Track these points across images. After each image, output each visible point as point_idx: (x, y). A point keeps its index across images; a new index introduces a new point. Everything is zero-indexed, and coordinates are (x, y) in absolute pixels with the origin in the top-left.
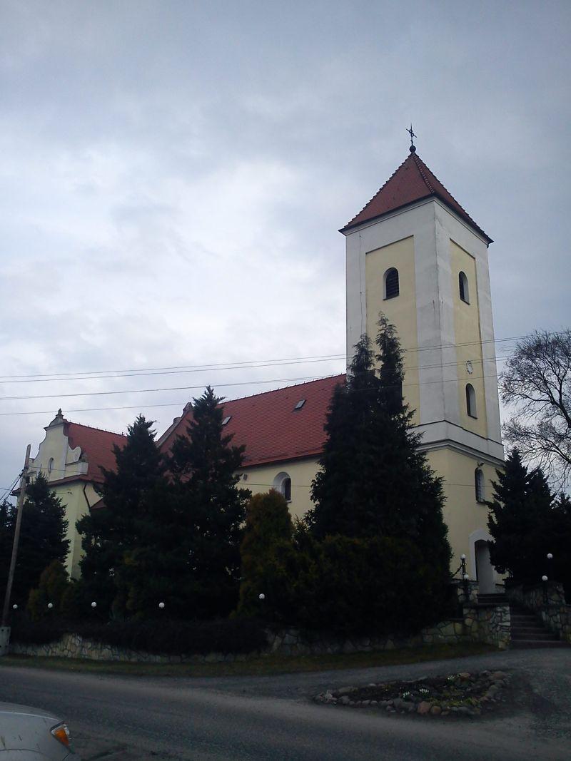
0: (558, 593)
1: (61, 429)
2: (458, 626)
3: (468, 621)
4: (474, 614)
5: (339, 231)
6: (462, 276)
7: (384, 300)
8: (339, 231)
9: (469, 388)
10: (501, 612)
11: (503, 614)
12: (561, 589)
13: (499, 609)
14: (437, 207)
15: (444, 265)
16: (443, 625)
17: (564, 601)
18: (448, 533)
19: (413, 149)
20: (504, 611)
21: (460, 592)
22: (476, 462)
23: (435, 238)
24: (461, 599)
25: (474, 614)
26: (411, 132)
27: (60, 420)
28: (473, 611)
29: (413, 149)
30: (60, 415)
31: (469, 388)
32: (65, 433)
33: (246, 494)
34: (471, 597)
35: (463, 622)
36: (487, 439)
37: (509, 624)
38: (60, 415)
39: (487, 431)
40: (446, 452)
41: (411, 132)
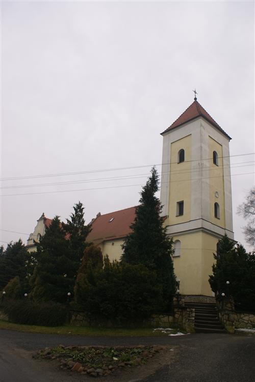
0: (231, 303)
1: (42, 221)
2: (171, 318)
3: (176, 316)
4: (180, 312)
5: (161, 134)
6: (215, 153)
7: (178, 163)
8: (161, 134)
9: (216, 205)
10: (189, 311)
11: (191, 313)
12: (233, 301)
13: (188, 310)
14: (201, 121)
15: (205, 147)
16: (162, 316)
17: (233, 308)
18: (174, 270)
19: (195, 99)
20: (192, 311)
21: (175, 299)
22: (218, 240)
23: (201, 135)
24: (175, 303)
25: (180, 312)
26: (195, 92)
27: (43, 217)
28: (180, 310)
29: (195, 99)
30: (43, 215)
31: (216, 205)
32: (44, 223)
33: (214, 274)
34: (181, 303)
35: (174, 316)
36: (225, 229)
37: (193, 318)
38: (43, 215)
39: (225, 225)
40: (201, 233)
41: (195, 92)
